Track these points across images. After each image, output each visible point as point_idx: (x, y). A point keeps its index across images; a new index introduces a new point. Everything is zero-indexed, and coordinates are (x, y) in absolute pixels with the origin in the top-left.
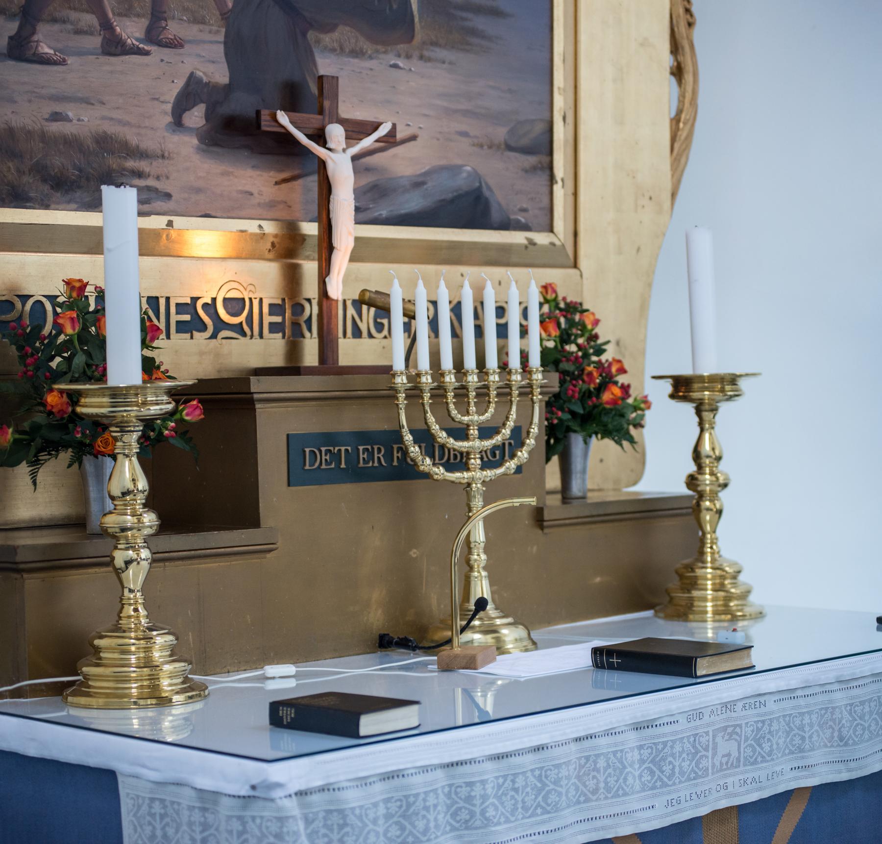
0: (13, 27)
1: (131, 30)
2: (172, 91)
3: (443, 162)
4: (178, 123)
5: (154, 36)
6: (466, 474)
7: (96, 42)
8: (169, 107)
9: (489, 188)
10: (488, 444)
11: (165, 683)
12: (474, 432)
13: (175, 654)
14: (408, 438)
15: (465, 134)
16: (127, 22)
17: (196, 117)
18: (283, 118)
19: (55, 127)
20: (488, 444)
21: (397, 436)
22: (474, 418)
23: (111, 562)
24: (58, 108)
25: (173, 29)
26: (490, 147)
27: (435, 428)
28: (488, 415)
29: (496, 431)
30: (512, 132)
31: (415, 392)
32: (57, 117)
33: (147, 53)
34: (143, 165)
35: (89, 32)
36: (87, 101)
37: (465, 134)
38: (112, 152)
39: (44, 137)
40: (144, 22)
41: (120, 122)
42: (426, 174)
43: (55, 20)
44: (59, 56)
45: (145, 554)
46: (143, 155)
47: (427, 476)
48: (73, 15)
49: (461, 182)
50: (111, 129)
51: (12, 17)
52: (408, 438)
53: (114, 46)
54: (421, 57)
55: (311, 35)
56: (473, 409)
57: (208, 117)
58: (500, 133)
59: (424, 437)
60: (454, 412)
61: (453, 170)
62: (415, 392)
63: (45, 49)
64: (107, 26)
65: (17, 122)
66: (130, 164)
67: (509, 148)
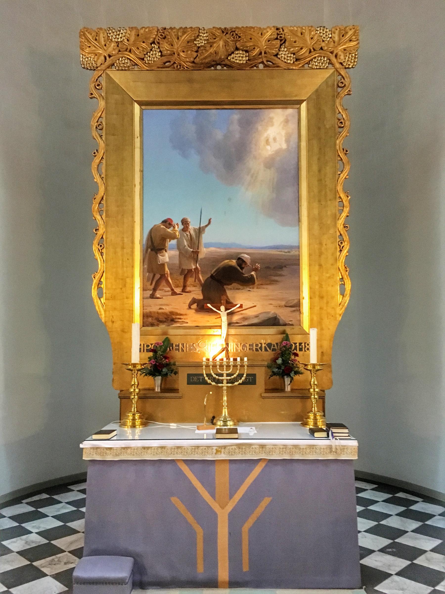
0: (151, 292)
1: (178, 290)
2: (188, 302)
3: (265, 311)
4: (190, 308)
5: (184, 291)
6: (222, 385)
7: (170, 293)
8: (188, 305)
9: (279, 316)
10: (229, 378)
11: (137, 423)
12: (225, 375)
13: (140, 418)
14: (205, 376)
15: (271, 304)
16: (177, 289)
17: (195, 306)
18: (209, 305)
19: (160, 311)
20: (229, 378)
21: (203, 375)
22: (225, 372)
23: (130, 398)
24: (161, 307)
25: (188, 289)
26: (279, 307)
27: (213, 374)
28: (231, 370)
29: (233, 375)
30: (287, 303)
31: (207, 366)
32: (160, 309)
33: (182, 294)
34: (181, 317)
35: (168, 291)
36: (168, 305)
37: (271, 304)
38: (173, 315)
39: (158, 313)
40: (182, 288)
41: (176, 309)
42: (260, 314)
43: (160, 290)
44: (161, 297)
45: (136, 397)
46: (181, 315)
47: (210, 384)
48: (165, 289)
49: (270, 315)
50: (173, 310)
51: (151, 290)
52: (205, 376)
53: (174, 293)
54: (257, 288)
55: (225, 287)
56: (225, 369)
57: (197, 306)
58: (283, 303)
59: (209, 375)
60: (218, 370)
61: (268, 313)
62: (207, 366)
63: (158, 296)
64: (172, 290)
65: (151, 310)
66: (178, 317)
67: (286, 306)
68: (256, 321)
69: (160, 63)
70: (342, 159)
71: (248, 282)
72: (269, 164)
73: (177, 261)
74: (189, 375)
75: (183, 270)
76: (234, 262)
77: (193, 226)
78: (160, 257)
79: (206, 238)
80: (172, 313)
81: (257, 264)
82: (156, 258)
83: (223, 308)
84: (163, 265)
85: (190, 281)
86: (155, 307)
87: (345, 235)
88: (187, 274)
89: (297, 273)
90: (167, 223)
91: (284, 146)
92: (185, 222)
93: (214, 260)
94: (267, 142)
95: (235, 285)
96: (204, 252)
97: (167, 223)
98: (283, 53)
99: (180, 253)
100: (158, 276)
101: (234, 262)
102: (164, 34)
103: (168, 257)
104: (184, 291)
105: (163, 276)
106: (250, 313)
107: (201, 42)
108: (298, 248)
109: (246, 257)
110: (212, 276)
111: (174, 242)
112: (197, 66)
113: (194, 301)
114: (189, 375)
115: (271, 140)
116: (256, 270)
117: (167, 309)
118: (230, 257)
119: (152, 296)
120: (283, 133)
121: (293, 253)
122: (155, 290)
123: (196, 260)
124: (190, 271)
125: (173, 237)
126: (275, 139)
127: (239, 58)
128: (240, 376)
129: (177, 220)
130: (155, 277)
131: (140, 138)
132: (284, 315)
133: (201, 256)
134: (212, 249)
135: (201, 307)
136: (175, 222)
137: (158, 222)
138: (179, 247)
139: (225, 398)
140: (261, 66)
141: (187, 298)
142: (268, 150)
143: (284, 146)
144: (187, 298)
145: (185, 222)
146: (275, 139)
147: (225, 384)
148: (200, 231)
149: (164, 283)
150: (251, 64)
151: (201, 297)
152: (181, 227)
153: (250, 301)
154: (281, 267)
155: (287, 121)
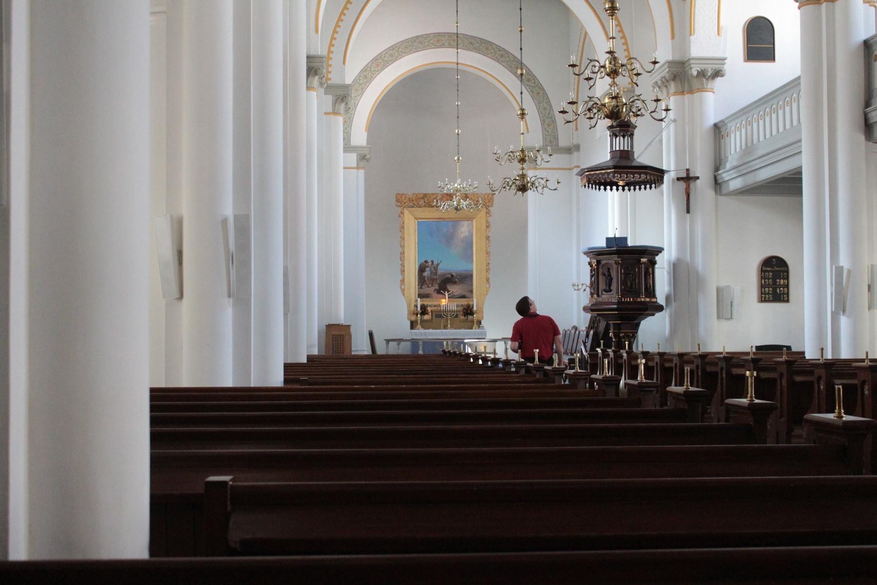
71: (455, 283)
81: (567, 382)
86: (422, 291)
87: (781, 393)
89: (472, 280)
90: (426, 262)
92: (432, 262)
93: (443, 275)
96: (439, 272)
97: (426, 262)
103: (427, 274)
105: (425, 281)
129: (430, 261)
130: (422, 281)
131: (531, 92)
135: (438, 292)
141: (433, 289)
142: (463, 235)
144: (433, 289)
145: (432, 262)
148: (438, 265)
153: (455, 289)
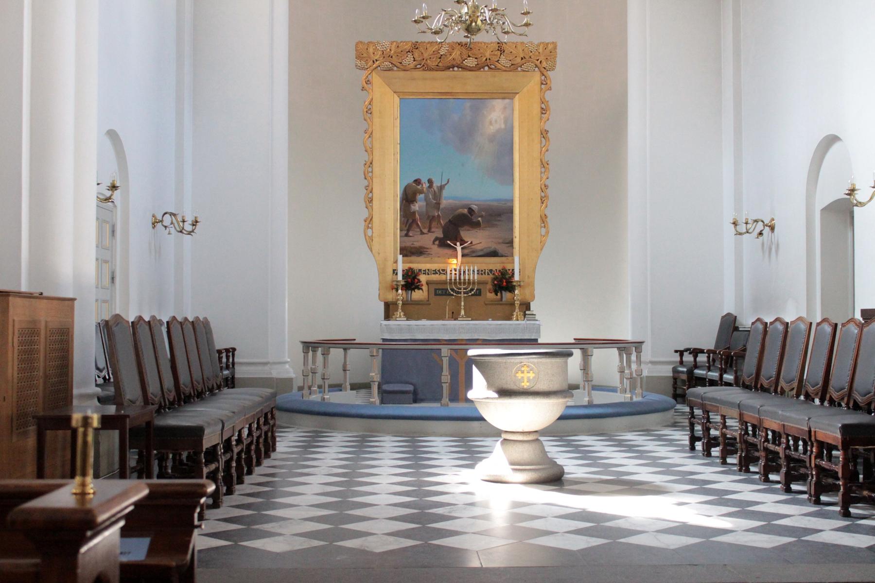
1: (425, 231)
2: (432, 239)
5: (429, 231)
17: (437, 242)
25: (433, 230)
53: (422, 233)
58: (501, 241)
59: (452, 290)
68: (481, 253)
69: (412, 66)
70: (580, 343)
71: (477, 225)
72: (492, 139)
73: (424, 209)
74: (436, 290)
75: (429, 217)
76: (466, 211)
77: (437, 184)
78: (412, 207)
79: (445, 193)
80: (421, 247)
82: (409, 207)
83: (458, 244)
84: (414, 213)
85: (434, 224)
88: (432, 219)
90: (418, 182)
91: (503, 126)
92: (430, 181)
93: (453, 209)
94: (491, 123)
95: (466, 227)
96: (444, 203)
98: (503, 60)
99: (427, 204)
100: (410, 221)
101: (466, 211)
102: (416, 46)
103: (418, 206)
104: (429, 231)
105: (414, 221)
106: (479, 247)
107: (442, 52)
108: (512, 201)
109: (474, 207)
110: (450, 221)
111: (422, 196)
112: (438, 69)
113: (436, 239)
114: (436, 290)
115: (493, 121)
116: (481, 216)
117: (417, 244)
118: (463, 207)
119: (407, 235)
120: (502, 117)
121: (509, 204)
122: (408, 230)
123: (438, 209)
124: (434, 217)
125: (421, 192)
126: (496, 121)
127: (471, 62)
128: (472, 290)
129: (424, 180)
130: (408, 221)
132: (501, 248)
133: (442, 206)
134: (450, 201)
136: (423, 181)
137: (411, 180)
138: (426, 199)
139: (463, 304)
140: (486, 68)
141: (432, 237)
142: (492, 129)
143: (503, 126)
145: (430, 181)
146: (496, 121)
147: (462, 295)
148: (441, 188)
149: (415, 226)
150: (478, 68)
151: (441, 235)
152: (428, 185)
154: (499, 215)
155: (505, 108)
